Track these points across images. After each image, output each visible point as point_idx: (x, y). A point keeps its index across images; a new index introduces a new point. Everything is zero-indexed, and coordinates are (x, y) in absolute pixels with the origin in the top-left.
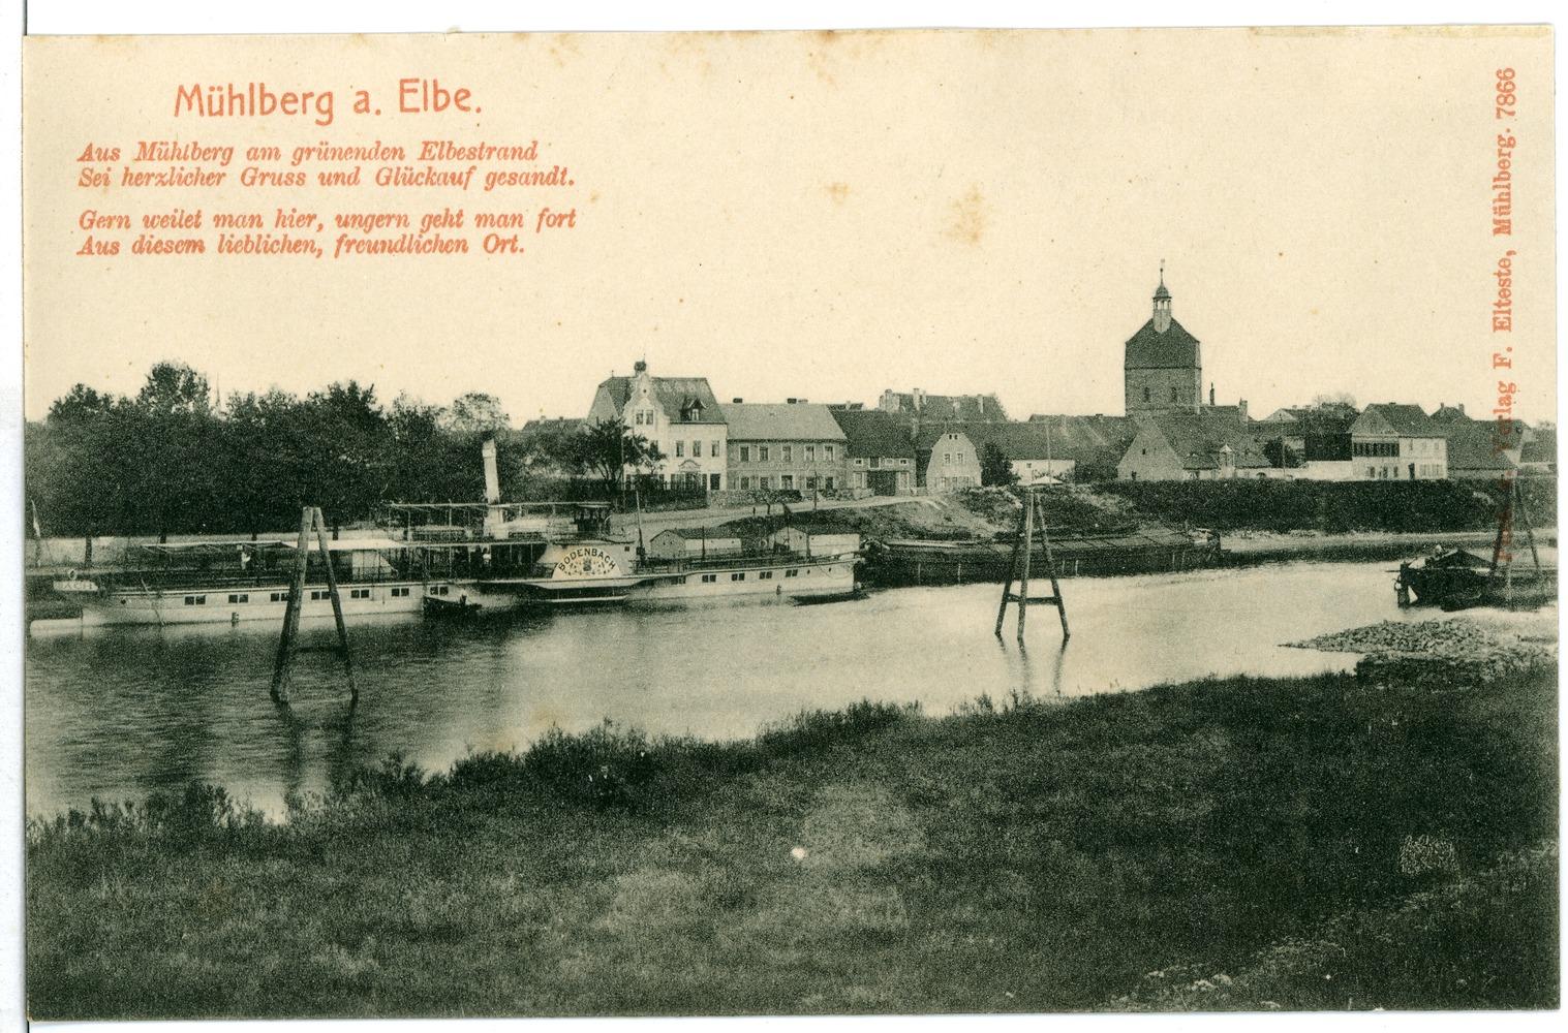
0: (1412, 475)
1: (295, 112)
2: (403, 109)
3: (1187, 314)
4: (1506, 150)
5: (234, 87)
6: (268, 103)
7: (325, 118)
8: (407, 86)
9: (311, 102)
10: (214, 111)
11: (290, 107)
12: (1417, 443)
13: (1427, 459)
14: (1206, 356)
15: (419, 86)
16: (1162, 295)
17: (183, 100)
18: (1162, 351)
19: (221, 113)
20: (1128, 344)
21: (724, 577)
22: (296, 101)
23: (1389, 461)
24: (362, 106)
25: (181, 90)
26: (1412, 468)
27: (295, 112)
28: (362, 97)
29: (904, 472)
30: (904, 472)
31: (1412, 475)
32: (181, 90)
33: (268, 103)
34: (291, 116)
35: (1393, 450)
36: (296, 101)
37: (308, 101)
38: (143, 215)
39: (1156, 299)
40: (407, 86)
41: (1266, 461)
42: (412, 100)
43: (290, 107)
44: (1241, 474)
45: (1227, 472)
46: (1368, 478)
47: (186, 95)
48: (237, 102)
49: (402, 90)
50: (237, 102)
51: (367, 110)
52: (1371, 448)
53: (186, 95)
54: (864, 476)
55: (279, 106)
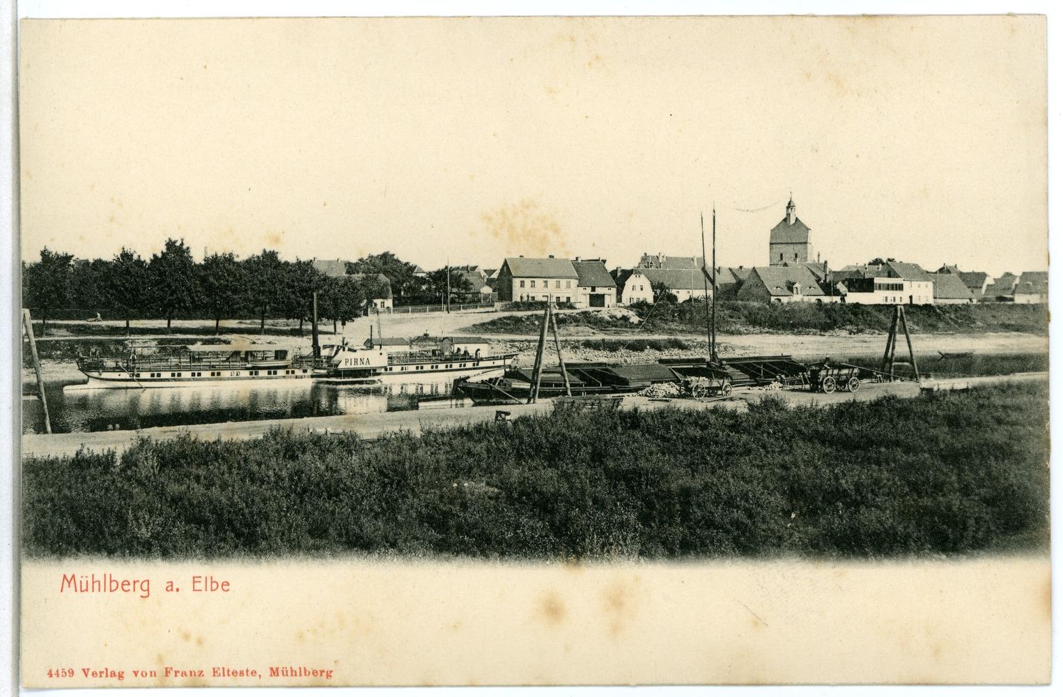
0: (911, 301)
1: (129, 590)
2: (194, 590)
3: (799, 213)
4: (324, 674)
5: (112, 576)
6: (114, 585)
7: (145, 594)
8: (196, 580)
9: (138, 585)
10: (83, 590)
11: (126, 588)
12: (915, 284)
13: (922, 293)
14: (812, 237)
15: (203, 580)
16: (790, 206)
17: (65, 581)
18: (789, 233)
19: (87, 590)
20: (386, 257)
21: (206, 404)
22: (129, 584)
23: (897, 294)
24: (169, 589)
25: (65, 577)
26: (911, 297)
27: (129, 590)
28: (170, 584)
29: (609, 295)
30: (609, 295)
31: (911, 301)
32: (65, 577)
33: (114, 585)
34: (226, 592)
35: (900, 287)
36: (129, 584)
37: (136, 584)
38: (298, 667)
39: (788, 208)
40: (196, 580)
41: (822, 293)
42: (198, 586)
43: (126, 588)
44: (806, 299)
45: (797, 298)
46: (885, 303)
47: (67, 580)
48: (96, 585)
49: (194, 582)
50: (96, 585)
51: (172, 590)
52: (886, 286)
53: (67, 580)
54: (588, 296)
55: (220, 587)
